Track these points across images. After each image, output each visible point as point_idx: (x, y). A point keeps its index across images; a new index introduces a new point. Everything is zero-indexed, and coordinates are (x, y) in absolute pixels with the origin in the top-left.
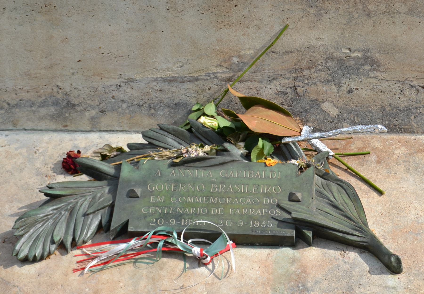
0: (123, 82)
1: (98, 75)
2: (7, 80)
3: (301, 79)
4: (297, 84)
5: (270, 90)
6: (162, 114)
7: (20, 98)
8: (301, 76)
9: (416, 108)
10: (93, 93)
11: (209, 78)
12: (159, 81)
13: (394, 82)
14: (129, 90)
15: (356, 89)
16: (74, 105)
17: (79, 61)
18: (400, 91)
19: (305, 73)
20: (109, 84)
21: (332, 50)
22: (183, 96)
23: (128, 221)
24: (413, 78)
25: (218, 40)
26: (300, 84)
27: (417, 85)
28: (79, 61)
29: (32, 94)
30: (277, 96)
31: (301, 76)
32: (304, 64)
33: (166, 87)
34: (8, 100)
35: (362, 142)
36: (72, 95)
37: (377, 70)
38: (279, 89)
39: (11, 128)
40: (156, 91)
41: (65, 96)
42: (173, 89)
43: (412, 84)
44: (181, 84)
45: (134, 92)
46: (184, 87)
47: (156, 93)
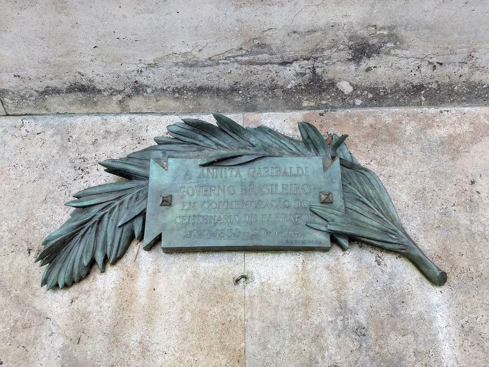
0: (144, 67)
1: (118, 61)
2: (28, 68)
3: (321, 59)
4: (316, 64)
5: (289, 72)
6: (186, 97)
7: (46, 85)
8: (321, 57)
9: (429, 83)
10: (116, 79)
11: (229, 62)
12: (180, 66)
13: (414, 59)
14: (151, 75)
15: (374, 67)
16: (100, 91)
17: (95, 47)
18: (417, 68)
19: (325, 53)
20: (130, 69)
21: (356, 28)
22: (205, 80)
23: (160, 235)
24: (433, 54)
25: (237, 20)
26: (320, 64)
27: (435, 61)
28: (95, 47)
29: (57, 81)
30: (295, 78)
31: (321, 57)
32: (326, 43)
33: (188, 71)
34: (36, 88)
35: (373, 118)
36: (96, 81)
37: (398, 48)
38: (298, 70)
39: (45, 112)
40: (178, 76)
41: (89, 83)
42: (195, 73)
43: (430, 61)
44: (202, 68)
45: (156, 77)
46: (205, 71)
47: (178, 77)
